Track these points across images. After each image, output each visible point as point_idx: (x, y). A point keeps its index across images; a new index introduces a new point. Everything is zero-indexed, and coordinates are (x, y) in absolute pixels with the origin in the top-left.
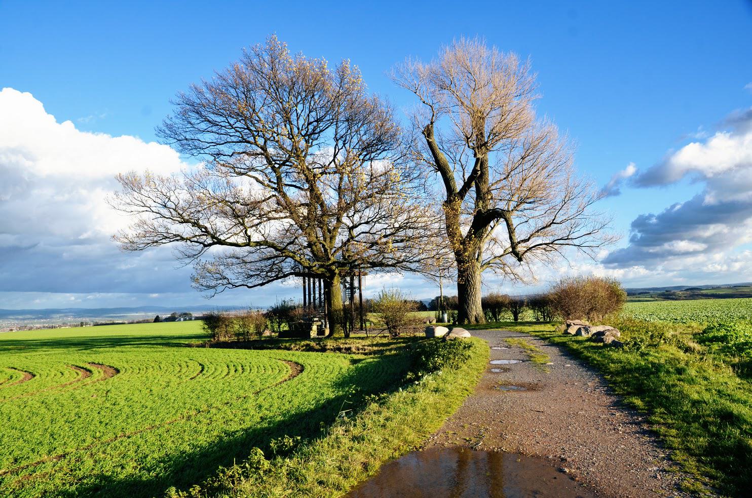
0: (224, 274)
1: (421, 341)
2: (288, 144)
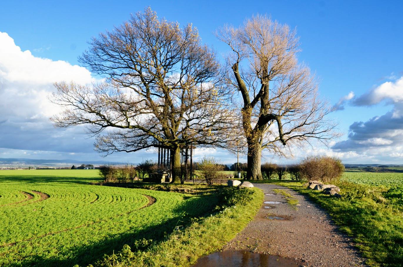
0: (113, 143)
2: (154, 70)
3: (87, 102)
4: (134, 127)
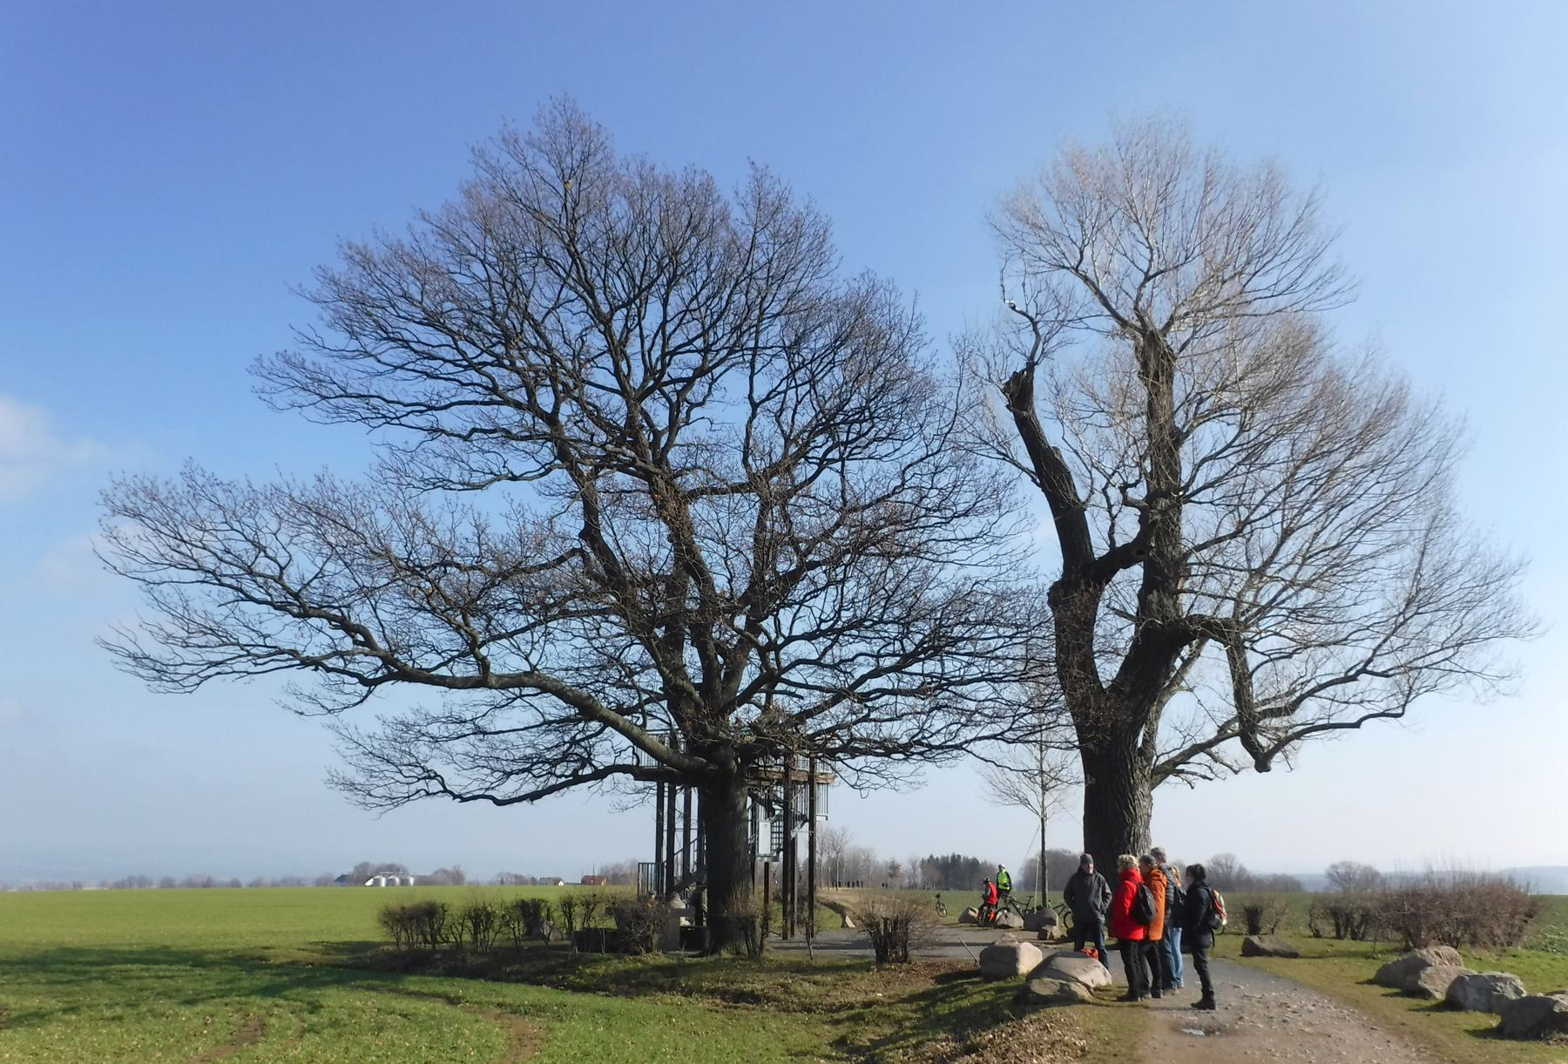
0: (428, 766)
1: (960, 981)
2: (615, 406)
3: (282, 569)
4: (506, 683)
